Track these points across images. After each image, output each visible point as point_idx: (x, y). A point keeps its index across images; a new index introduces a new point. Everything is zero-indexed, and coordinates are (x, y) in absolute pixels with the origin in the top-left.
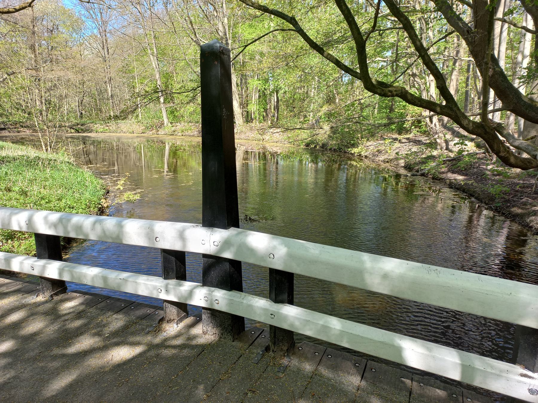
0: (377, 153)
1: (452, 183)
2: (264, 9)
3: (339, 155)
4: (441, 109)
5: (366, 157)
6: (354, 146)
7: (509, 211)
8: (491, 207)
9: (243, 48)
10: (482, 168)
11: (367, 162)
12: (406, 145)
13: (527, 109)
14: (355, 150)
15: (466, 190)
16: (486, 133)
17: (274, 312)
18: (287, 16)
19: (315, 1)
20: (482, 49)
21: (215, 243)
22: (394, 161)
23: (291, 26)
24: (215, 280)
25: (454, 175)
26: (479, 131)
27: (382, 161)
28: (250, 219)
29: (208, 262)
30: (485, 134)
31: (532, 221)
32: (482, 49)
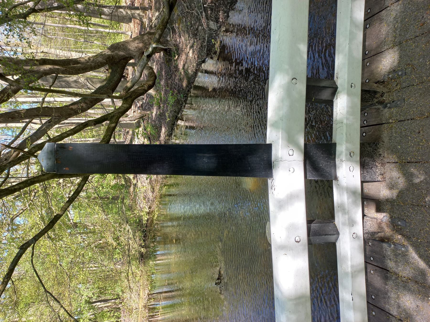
0: (146, 200)
1: (167, 134)
2: (7, 278)
3: (149, 232)
4: (113, 123)
5: (150, 208)
6: (141, 221)
7: (186, 87)
8: (184, 101)
9: (48, 294)
10: (155, 119)
11: (154, 207)
12: (139, 178)
13: (112, 82)
14: (145, 218)
15: (173, 123)
16: (130, 97)
17: (348, 83)
18: (18, 254)
19: (1, 107)
20: (65, 111)
21: (291, 153)
22: (153, 184)
23: (30, 249)
24: (328, 162)
25: (162, 135)
26: (130, 100)
27: (153, 194)
28: (218, 279)
29: (310, 171)
30: (131, 97)
31: (192, 71)
32: (65, 111)
